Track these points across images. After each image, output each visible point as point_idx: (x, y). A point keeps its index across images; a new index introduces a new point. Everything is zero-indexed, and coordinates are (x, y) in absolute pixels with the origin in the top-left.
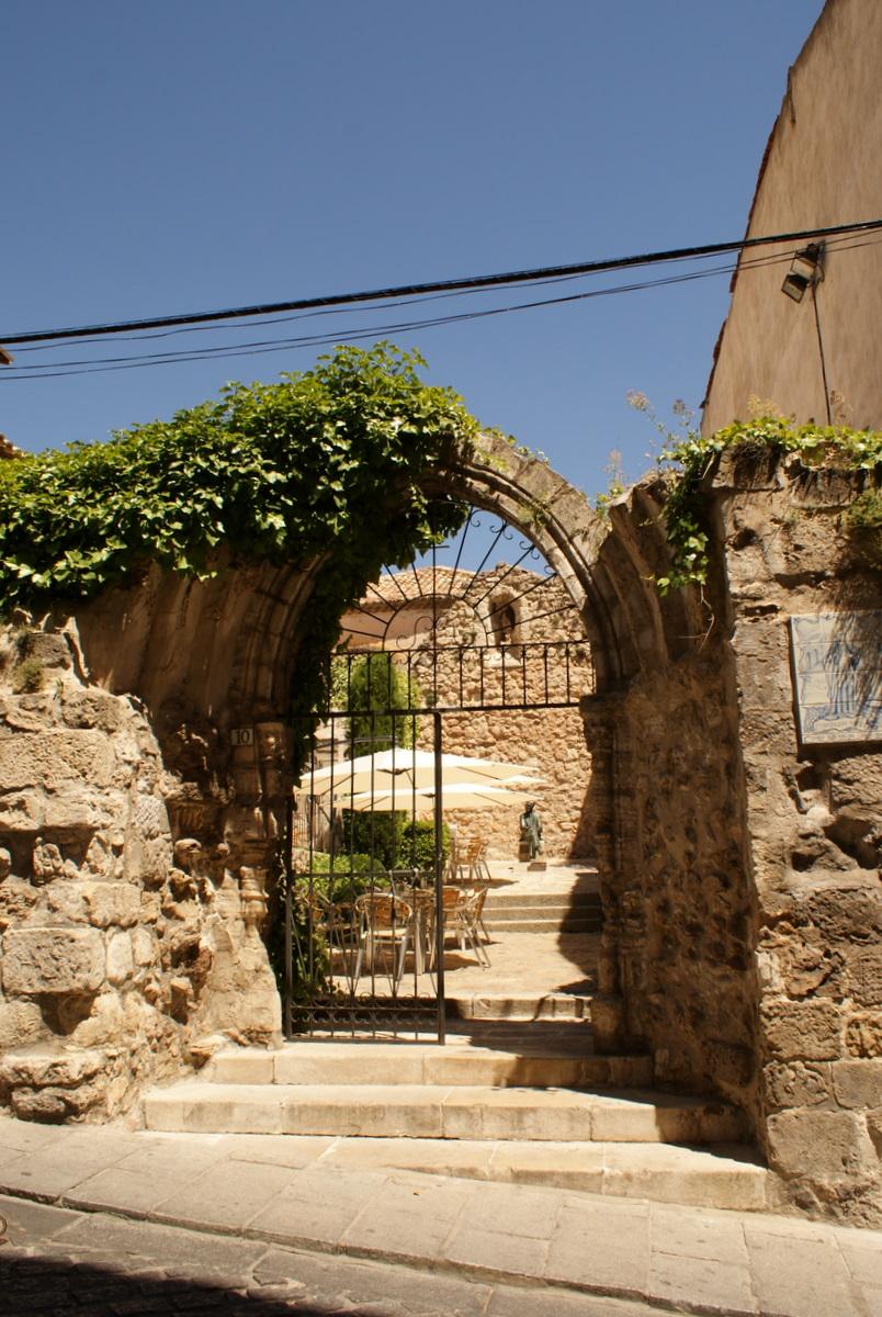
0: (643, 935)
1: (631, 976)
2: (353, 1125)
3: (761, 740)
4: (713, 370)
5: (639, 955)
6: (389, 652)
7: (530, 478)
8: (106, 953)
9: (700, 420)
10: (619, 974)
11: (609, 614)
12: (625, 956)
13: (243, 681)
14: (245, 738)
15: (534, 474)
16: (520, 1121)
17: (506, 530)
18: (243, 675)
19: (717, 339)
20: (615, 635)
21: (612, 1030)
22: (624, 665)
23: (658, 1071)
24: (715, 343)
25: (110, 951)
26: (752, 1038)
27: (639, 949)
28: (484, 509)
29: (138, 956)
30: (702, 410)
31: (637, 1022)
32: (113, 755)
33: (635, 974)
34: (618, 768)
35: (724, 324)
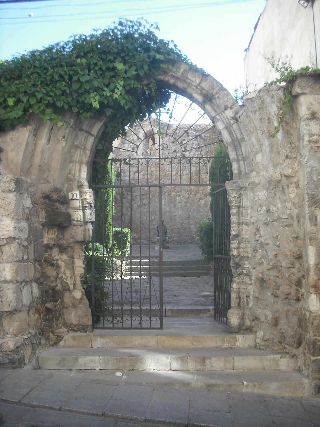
0: (251, 284)
1: (246, 301)
2: (132, 366)
3: (316, 204)
4: (253, 35)
5: (249, 292)
6: (139, 159)
7: (206, 83)
8: (22, 294)
9: (244, 57)
10: (240, 301)
11: (240, 145)
12: (243, 293)
13: (74, 171)
14: (75, 197)
15: (208, 81)
16: (204, 362)
17: (192, 105)
18: (74, 168)
19: (257, 21)
20: (242, 155)
21: (238, 324)
22: (246, 168)
23: (258, 341)
24: (255, 23)
25: (23, 294)
26: (18, 251)
27: (249, 290)
28: (182, 95)
29: (34, 295)
30: (245, 52)
31: (247, 320)
32: (22, 205)
33: (247, 301)
34: (243, 213)
35: (261, 15)
